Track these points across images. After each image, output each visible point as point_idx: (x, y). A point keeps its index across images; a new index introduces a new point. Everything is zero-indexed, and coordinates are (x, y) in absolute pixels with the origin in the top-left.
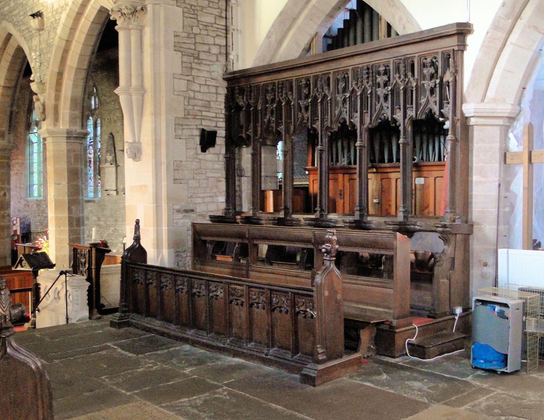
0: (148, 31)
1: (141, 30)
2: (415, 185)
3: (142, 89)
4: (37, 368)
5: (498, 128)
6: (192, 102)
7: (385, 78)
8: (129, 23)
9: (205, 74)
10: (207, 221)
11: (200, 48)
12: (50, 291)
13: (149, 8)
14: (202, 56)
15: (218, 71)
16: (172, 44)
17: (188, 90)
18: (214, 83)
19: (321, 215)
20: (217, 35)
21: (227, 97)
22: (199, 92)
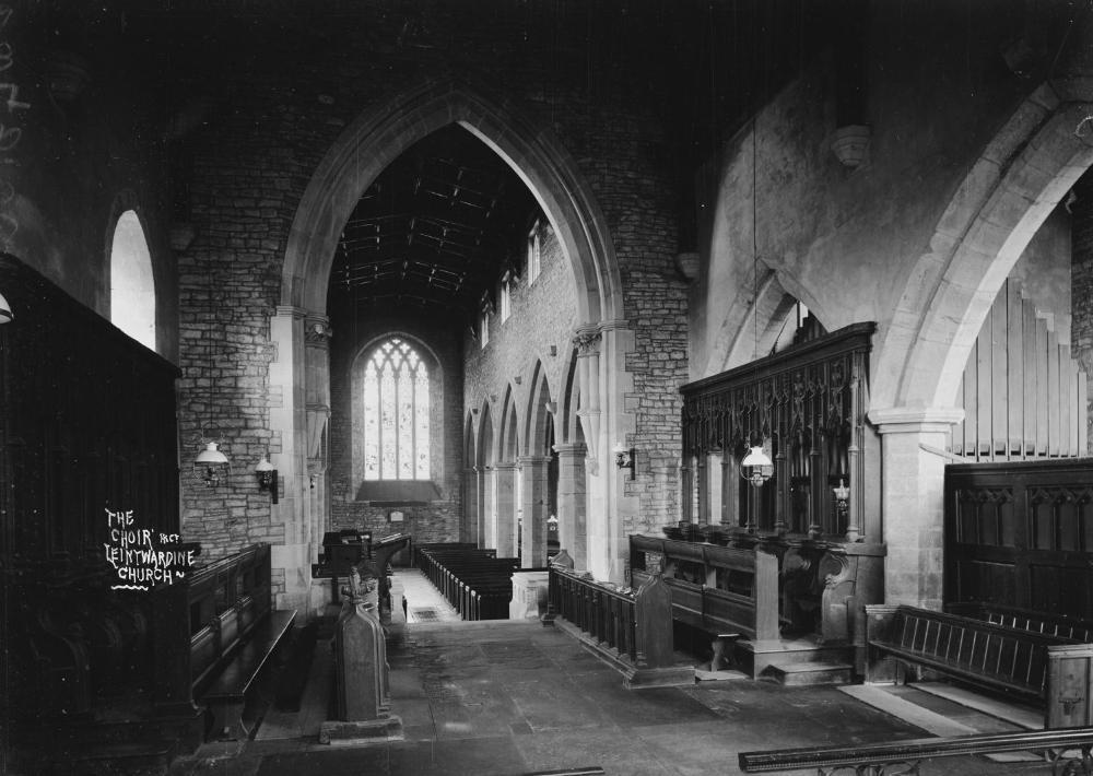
0: (603, 356)
1: (598, 355)
2: (751, 487)
3: (598, 410)
4: (339, 347)
5: (943, 436)
6: (645, 418)
7: (801, 385)
8: (588, 351)
9: (660, 390)
10: (663, 536)
11: (653, 365)
12: (400, 444)
13: (604, 334)
14: (657, 372)
15: (673, 385)
16: (623, 366)
17: (641, 406)
18: (669, 397)
19: (751, 531)
20: (673, 351)
21: (684, 410)
22: (653, 407)
